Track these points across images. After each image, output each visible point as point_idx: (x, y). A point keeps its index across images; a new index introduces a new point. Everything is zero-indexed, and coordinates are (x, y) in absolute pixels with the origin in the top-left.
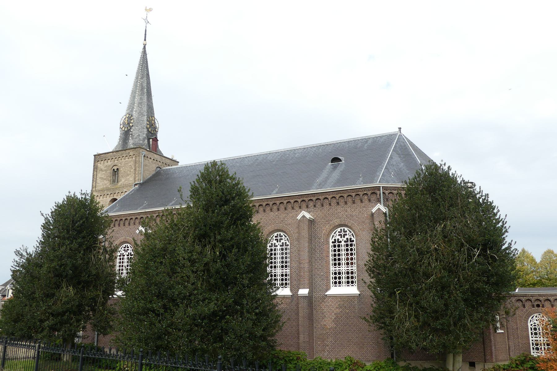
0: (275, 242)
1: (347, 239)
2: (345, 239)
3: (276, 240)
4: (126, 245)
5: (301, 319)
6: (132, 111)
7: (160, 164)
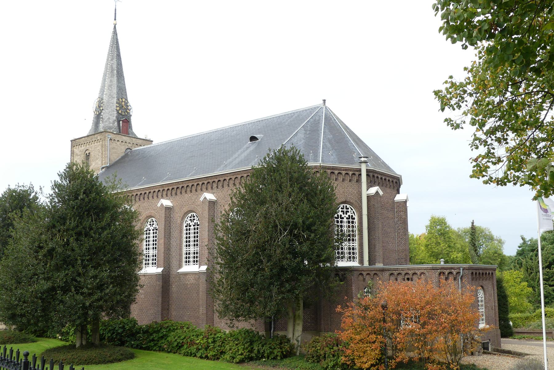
0: (340, 213)
2: (347, 216)
3: (342, 211)
4: (192, 214)
6: (103, 94)
7: (130, 145)
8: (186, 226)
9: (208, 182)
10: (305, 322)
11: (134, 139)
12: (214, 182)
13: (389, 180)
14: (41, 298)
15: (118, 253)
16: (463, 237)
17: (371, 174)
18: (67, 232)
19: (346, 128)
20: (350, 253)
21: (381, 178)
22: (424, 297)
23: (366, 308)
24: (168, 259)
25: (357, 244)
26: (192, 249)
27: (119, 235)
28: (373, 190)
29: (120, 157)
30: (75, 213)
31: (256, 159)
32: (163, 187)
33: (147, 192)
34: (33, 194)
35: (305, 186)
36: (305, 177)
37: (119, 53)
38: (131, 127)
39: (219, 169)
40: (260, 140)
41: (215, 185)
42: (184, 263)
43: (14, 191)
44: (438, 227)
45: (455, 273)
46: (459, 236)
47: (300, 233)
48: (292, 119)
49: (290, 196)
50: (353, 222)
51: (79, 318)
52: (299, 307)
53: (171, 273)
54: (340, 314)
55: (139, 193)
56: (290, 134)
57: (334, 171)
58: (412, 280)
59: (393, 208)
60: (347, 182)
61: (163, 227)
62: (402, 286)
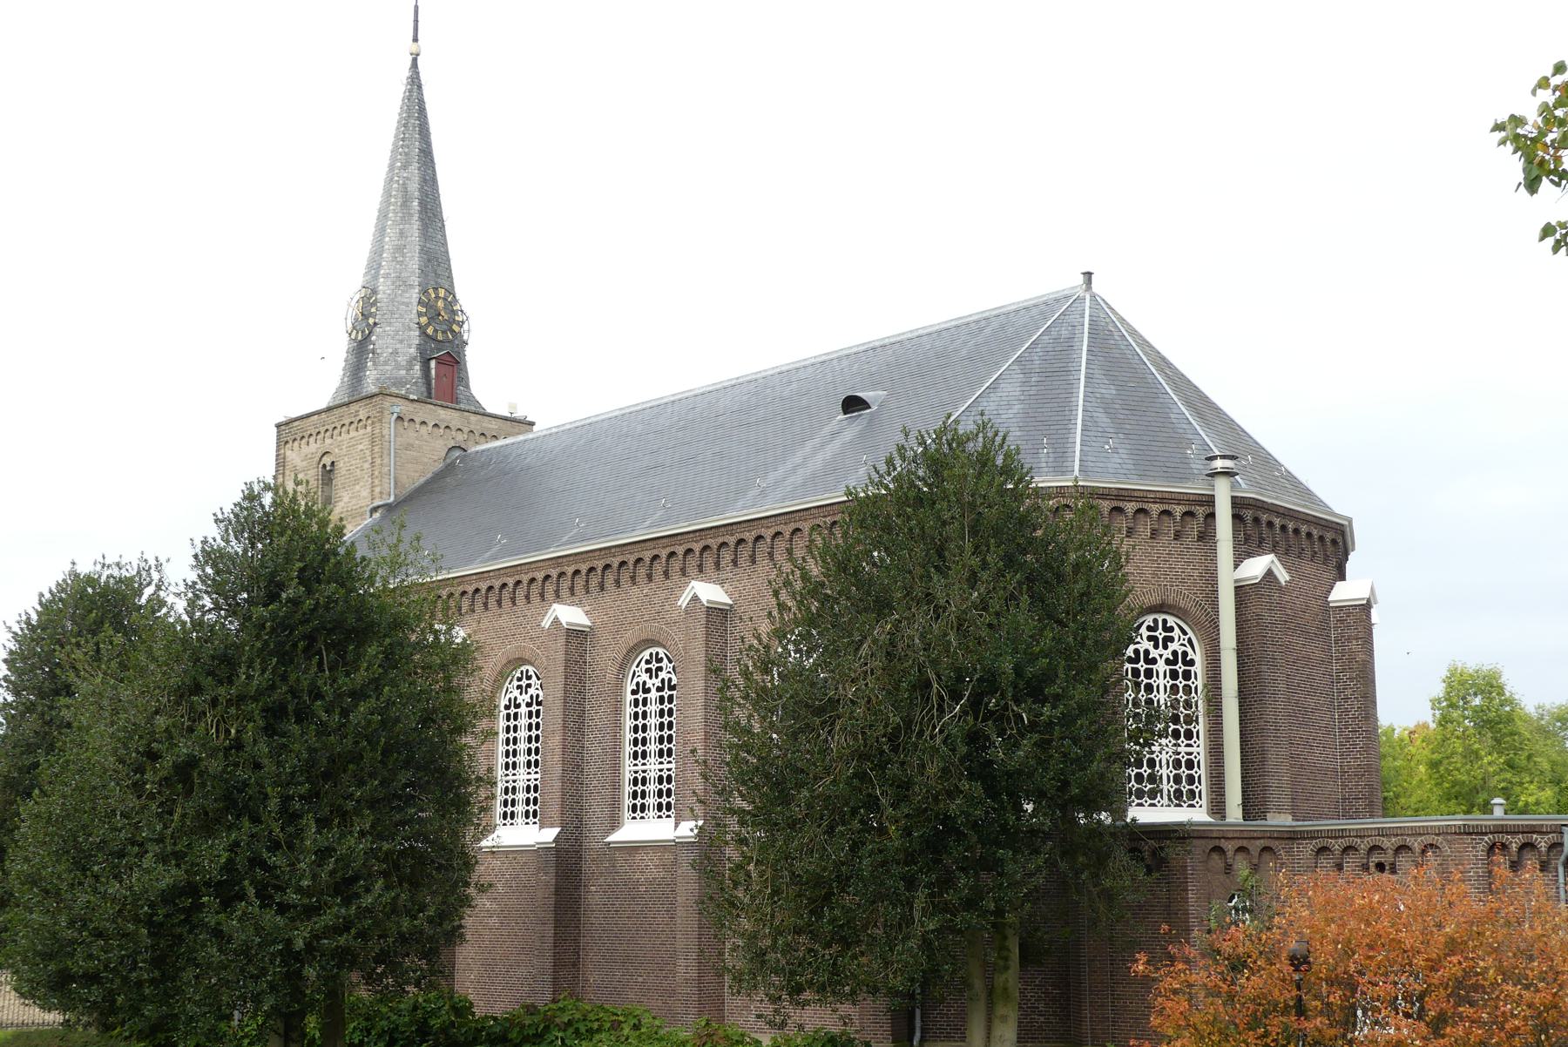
0: (1146, 645)
1: (1175, 653)
2: (1168, 654)
3: (1150, 638)
4: (653, 650)
5: (680, 912)
6: (375, 277)
7: (460, 437)
8: (634, 692)
9: (706, 548)
10: (1026, 1011)
11: (473, 418)
12: (724, 544)
13: (1309, 535)
14: (149, 922)
15: (404, 776)
16: (1556, 735)
17: (1248, 514)
18: (238, 708)
19: (1163, 363)
20: (1177, 779)
21: (1283, 528)
22: (1440, 926)
23: (1237, 965)
24: (576, 800)
25: (1201, 750)
26: (653, 767)
27: (407, 717)
28: (1255, 567)
29: (429, 475)
30: (266, 643)
31: (862, 471)
32: (559, 565)
33: (511, 582)
34: (148, 591)
35: (1024, 552)
36: (1023, 521)
37: (429, 144)
38: (464, 380)
39: (740, 504)
40: (874, 408)
41: (727, 556)
42: (627, 814)
43: (90, 580)
44: (1477, 701)
45: (1543, 846)
46: (1543, 732)
47: (1006, 708)
48: (980, 339)
49: (973, 580)
50: (1187, 675)
51: (273, 987)
52: (1006, 959)
53: (586, 844)
54: (1147, 982)
55: (483, 586)
56: (973, 387)
57: (1121, 504)
58: (1393, 871)
59: (1324, 628)
60: (1166, 539)
61: (560, 694)
62: (1363, 891)
